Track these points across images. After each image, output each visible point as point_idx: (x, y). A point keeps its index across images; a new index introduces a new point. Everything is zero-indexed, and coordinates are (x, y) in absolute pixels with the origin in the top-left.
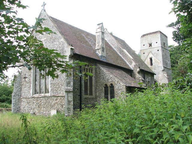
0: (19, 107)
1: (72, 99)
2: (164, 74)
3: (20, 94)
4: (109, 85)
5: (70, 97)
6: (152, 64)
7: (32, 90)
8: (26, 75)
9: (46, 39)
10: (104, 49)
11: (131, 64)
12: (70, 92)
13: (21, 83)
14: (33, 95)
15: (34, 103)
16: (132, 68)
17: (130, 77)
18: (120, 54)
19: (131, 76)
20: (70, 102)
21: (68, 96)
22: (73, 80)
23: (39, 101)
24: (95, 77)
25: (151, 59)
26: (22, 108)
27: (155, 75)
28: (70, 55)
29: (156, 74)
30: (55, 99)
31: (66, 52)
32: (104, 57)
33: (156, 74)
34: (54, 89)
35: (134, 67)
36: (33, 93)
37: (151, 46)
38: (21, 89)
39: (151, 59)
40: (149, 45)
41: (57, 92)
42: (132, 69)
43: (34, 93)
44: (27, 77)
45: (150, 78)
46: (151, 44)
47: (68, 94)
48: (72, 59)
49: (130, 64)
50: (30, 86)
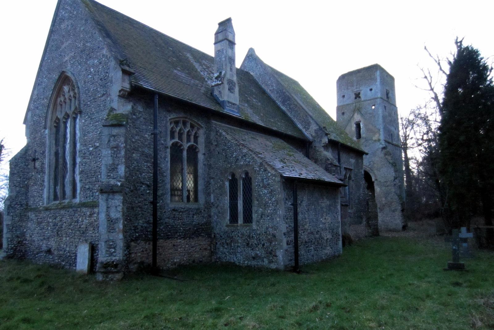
0: (23, 234)
1: (119, 215)
2: (387, 157)
3: (24, 202)
4: (240, 175)
5: (113, 209)
6: (359, 136)
7: (46, 190)
8: (37, 154)
9: (72, 54)
10: (234, 86)
11: (307, 129)
12: (114, 192)
13: (28, 173)
14: (49, 203)
15: (49, 222)
16: (106, 40)
17: (306, 159)
18: (284, 105)
19: (307, 155)
20: (115, 223)
21: (108, 204)
22: (124, 160)
23: (58, 219)
24: (204, 154)
25: (358, 125)
26: (28, 235)
27: (364, 156)
28: (120, 91)
29: (367, 154)
30: (88, 213)
31: (111, 82)
32: (234, 104)
33: (367, 154)
34: (87, 187)
35: (314, 134)
36: (49, 198)
37: (360, 97)
38: (27, 187)
39: (358, 125)
40: (354, 96)
41: (93, 193)
42: (310, 138)
43: (52, 197)
44: (38, 159)
45: (353, 161)
46: (359, 93)
47: (107, 200)
48: (130, 101)
49: (305, 127)
50: (43, 181)
